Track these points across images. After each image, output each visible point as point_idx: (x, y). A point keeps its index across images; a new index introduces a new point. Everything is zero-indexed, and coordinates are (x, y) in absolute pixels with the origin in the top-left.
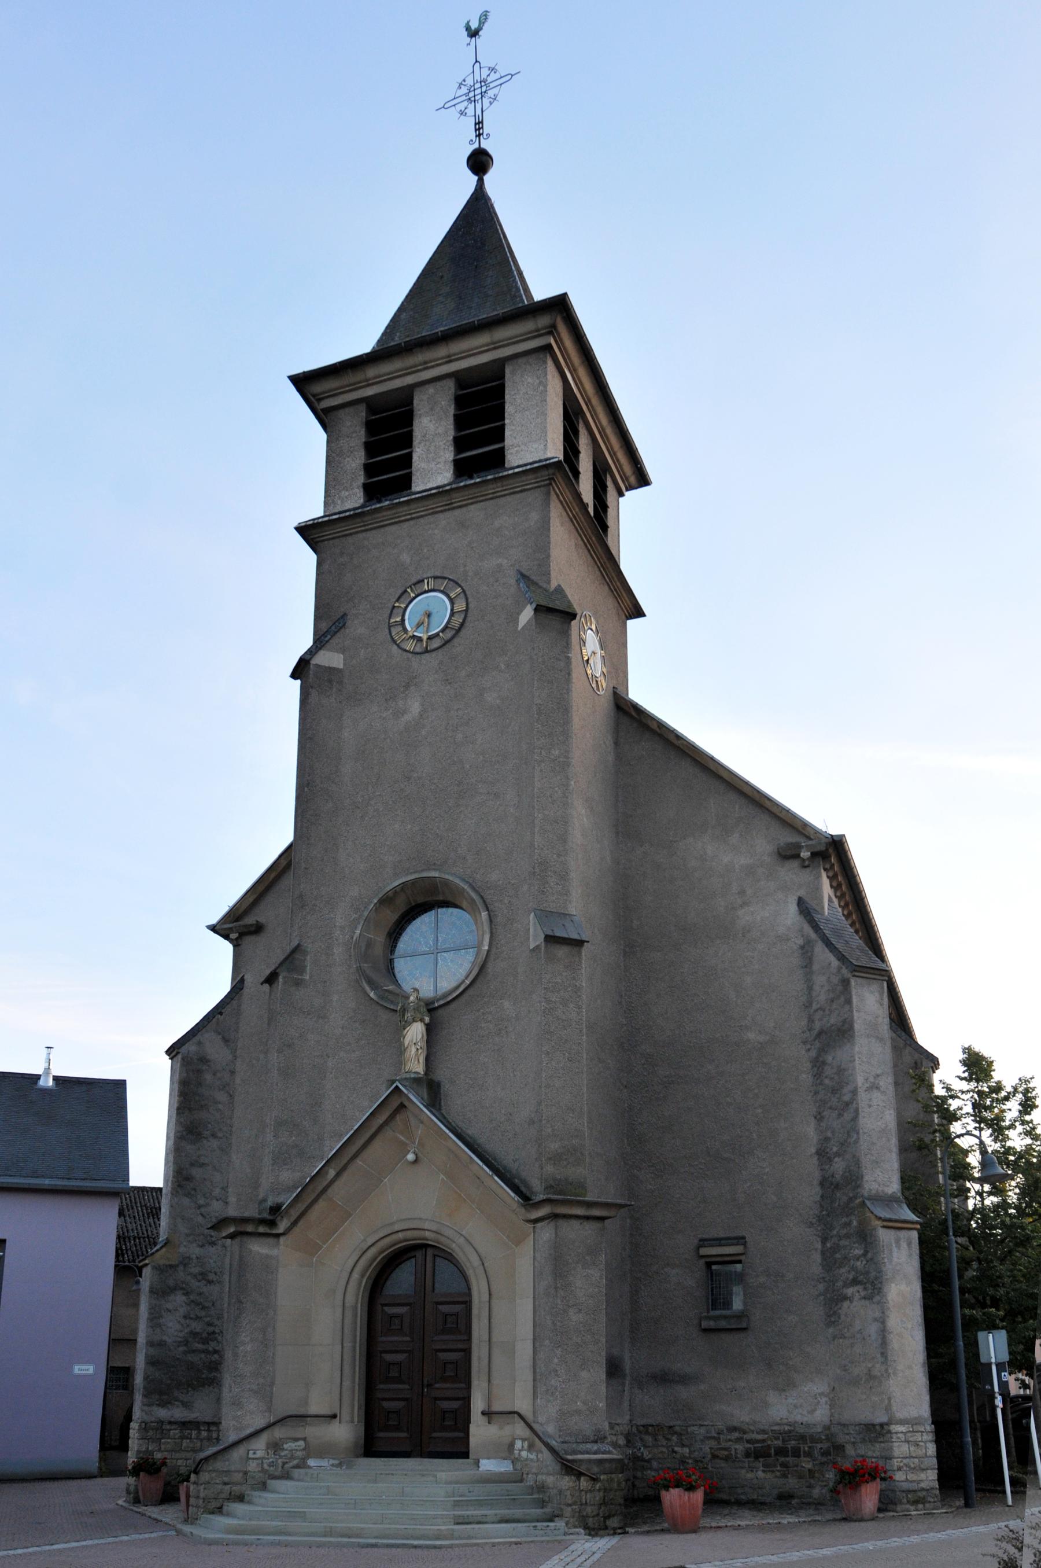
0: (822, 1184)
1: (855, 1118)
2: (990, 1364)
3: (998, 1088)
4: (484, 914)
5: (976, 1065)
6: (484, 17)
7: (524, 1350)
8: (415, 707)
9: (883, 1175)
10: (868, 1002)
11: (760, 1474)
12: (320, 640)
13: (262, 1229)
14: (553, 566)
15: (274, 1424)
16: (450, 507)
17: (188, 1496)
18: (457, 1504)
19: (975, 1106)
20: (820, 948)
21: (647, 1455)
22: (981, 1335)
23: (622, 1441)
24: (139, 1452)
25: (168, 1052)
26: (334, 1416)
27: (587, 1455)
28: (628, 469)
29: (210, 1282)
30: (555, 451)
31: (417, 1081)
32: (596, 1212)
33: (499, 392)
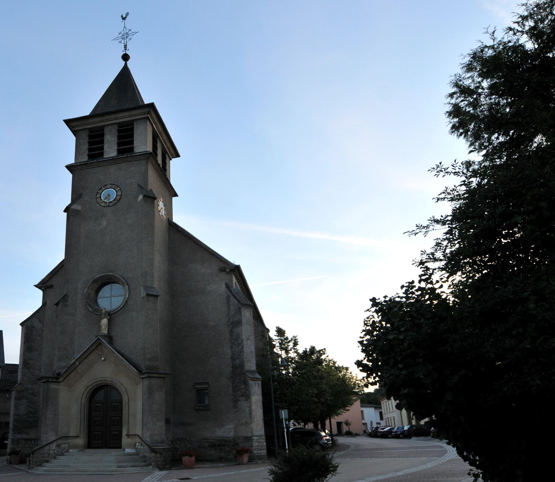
0: (232, 367)
1: (243, 347)
2: (282, 419)
3: (287, 338)
4: (127, 286)
5: (280, 332)
6: (127, 14)
7: (139, 416)
8: (105, 223)
9: (251, 365)
10: (247, 314)
11: (213, 452)
12: (74, 201)
13: (54, 380)
14: (149, 183)
15: (58, 439)
16: (116, 163)
17: (29, 461)
18: (118, 462)
19: (280, 344)
20: (232, 298)
21: (178, 447)
22: (280, 411)
23: (170, 443)
24: (11, 448)
25: (21, 324)
26: (78, 437)
27: (160, 447)
28: (173, 152)
29: (35, 396)
30: (150, 149)
31: (105, 336)
32: (162, 376)
33: (132, 129)
